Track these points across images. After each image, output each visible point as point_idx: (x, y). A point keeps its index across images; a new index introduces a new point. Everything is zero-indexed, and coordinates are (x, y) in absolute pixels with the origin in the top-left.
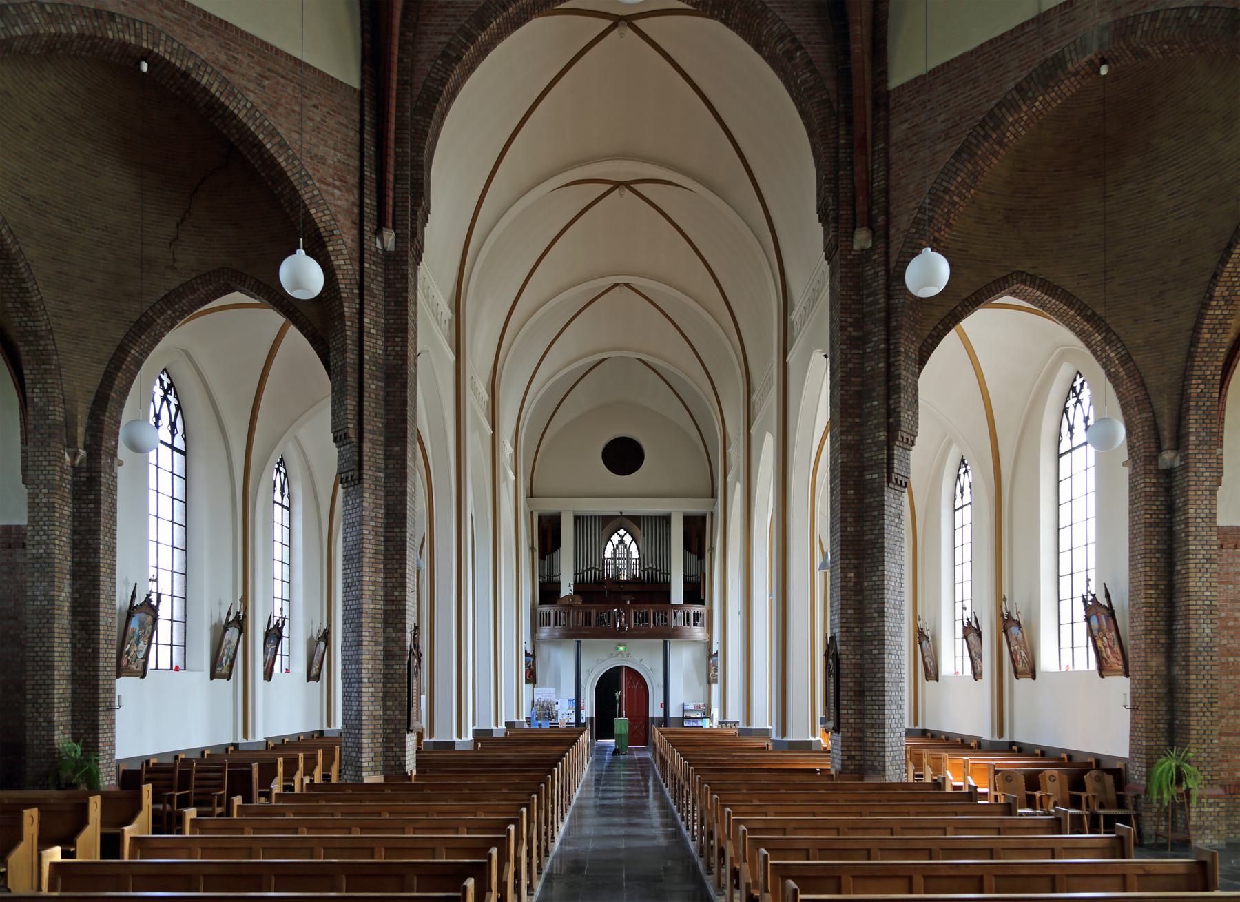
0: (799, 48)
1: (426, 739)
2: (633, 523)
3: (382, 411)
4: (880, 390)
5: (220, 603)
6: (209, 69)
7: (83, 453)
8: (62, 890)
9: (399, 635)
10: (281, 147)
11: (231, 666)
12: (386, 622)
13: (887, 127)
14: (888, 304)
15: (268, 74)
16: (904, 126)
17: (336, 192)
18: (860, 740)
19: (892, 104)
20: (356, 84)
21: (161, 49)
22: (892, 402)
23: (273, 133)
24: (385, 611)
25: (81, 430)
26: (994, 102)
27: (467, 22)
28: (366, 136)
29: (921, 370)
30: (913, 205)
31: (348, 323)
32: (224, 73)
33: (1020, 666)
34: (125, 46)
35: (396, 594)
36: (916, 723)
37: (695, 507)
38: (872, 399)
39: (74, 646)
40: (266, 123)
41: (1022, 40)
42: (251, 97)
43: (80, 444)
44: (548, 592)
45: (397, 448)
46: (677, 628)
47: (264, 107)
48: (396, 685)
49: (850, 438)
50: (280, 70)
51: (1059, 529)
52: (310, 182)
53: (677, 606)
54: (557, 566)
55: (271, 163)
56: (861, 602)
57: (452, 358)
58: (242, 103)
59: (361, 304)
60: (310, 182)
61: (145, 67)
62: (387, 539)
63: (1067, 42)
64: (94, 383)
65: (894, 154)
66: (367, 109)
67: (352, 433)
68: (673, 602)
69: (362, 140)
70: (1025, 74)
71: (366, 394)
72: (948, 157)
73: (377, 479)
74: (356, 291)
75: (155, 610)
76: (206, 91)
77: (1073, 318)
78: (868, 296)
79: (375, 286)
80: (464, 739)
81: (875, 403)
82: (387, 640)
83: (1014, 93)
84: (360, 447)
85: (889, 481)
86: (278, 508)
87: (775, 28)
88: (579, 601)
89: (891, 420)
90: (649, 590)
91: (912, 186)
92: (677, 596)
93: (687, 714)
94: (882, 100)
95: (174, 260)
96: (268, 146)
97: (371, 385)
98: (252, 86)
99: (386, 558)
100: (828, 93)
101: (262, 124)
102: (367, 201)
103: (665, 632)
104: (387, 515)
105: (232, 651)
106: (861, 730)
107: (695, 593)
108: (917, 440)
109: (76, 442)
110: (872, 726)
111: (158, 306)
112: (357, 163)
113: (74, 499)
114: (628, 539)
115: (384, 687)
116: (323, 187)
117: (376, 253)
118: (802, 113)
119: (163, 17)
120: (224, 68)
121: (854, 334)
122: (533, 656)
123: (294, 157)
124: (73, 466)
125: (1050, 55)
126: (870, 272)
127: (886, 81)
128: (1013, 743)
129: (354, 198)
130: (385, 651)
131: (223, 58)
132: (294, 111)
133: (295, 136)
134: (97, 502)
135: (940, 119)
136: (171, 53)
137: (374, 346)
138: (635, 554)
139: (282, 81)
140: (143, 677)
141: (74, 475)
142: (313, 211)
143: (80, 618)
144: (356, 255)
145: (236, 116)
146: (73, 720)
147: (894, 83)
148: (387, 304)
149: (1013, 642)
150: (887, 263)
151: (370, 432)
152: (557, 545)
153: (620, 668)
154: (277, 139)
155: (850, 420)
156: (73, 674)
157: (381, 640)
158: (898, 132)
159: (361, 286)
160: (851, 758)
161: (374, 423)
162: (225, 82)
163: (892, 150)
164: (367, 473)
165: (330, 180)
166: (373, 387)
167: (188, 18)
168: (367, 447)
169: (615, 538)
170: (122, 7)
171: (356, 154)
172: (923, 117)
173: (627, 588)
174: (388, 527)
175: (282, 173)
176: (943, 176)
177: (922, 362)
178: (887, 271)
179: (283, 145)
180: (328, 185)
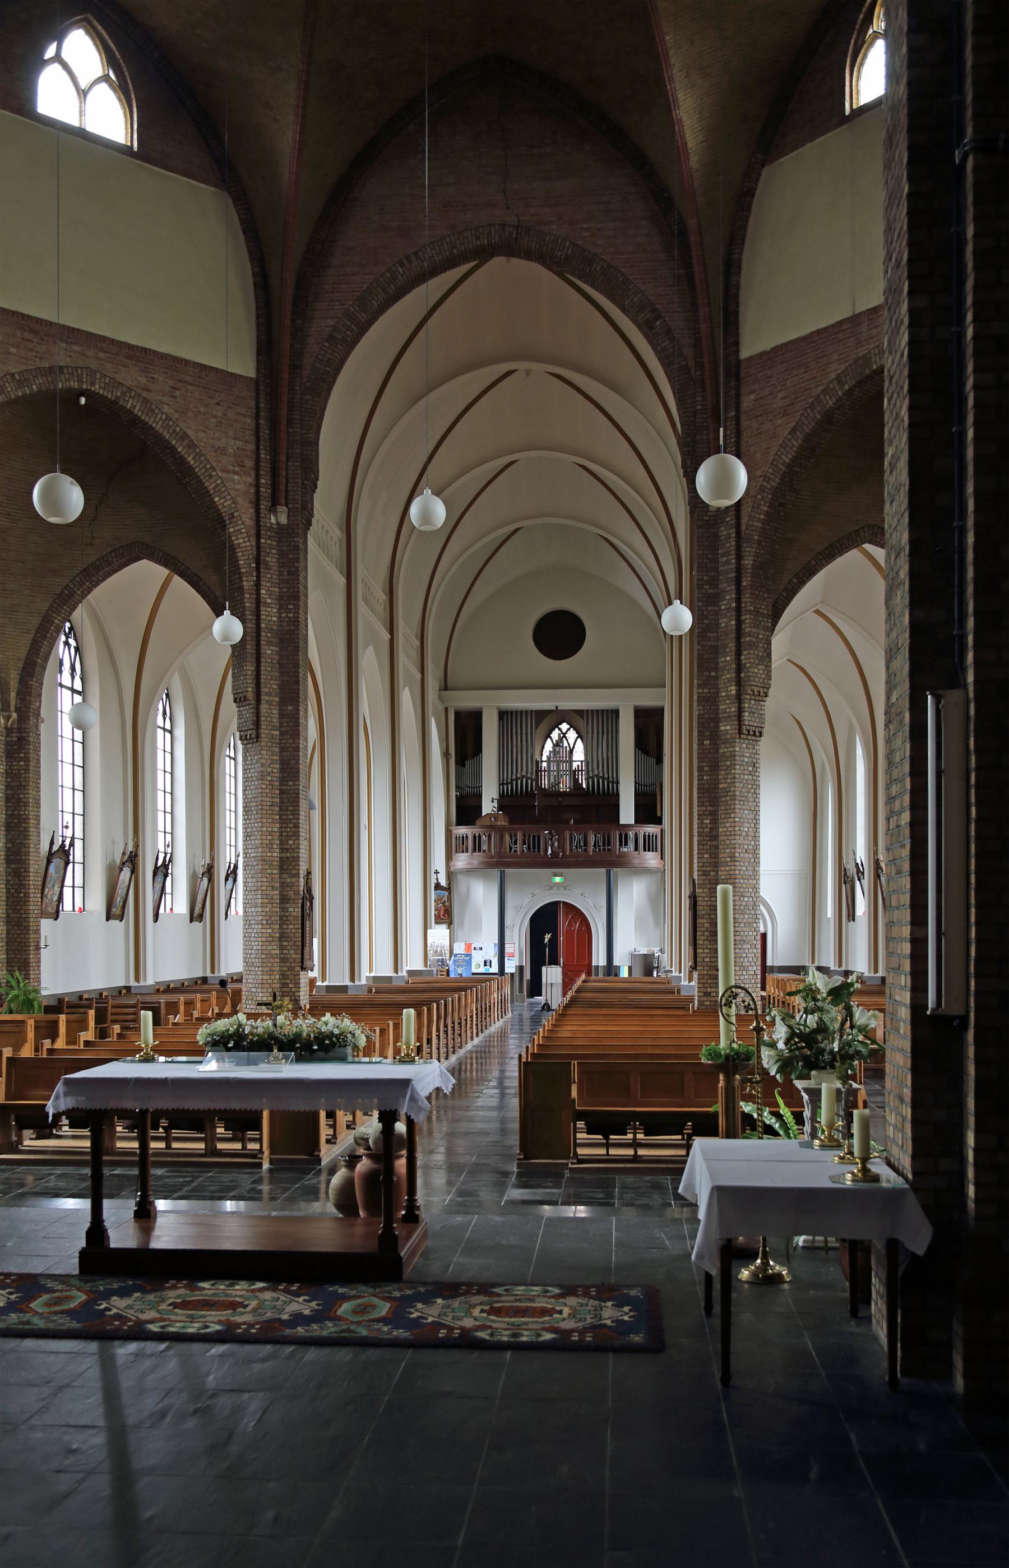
1: (319, 983)
2: (576, 718)
3: (277, 674)
4: (732, 645)
5: (113, 843)
6: (133, 394)
7: (15, 715)
9: (294, 880)
10: (190, 448)
11: (124, 907)
12: (282, 869)
13: (738, 396)
15: (179, 385)
16: (752, 397)
17: (236, 477)
19: (743, 374)
20: (252, 373)
21: (97, 386)
23: (184, 436)
24: (281, 858)
25: (13, 695)
26: (820, 388)
27: (351, 305)
28: (261, 422)
29: (775, 624)
31: (247, 596)
32: (145, 394)
34: (70, 390)
35: (290, 842)
36: (840, 965)
37: (648, 699)
38: (726, 654)
39: (8, 891)
40: (178, 429)
41: (840, 336)
42: (166, 409)
43: (12, 708)
44: (466, 810)
45: (290, 708)
47: (176, 416)
48: (291, 927)
49: (706, 690)
50: (189, 379)
52: (214, 474)
54: (478, 775)
55: (182, 461)
56: (717, 847)
57: (342, 580)
58: (159, 417)
59: (258, 576)
60: (214, 474)
61: (83, 401)
62: (282, 792)
63: (872, 346)
64: (23, 652)
65: (744, 423)
66: (262, 396)
67: (251, 695)
68: (623, 821)
69: (258, 425)
70: (843, 367)
71: (263, 660)
72: (786, 432)
73: (273, 737)
74: (254, 565)
75: (67, 854)
76: (130, 412)
77: (272, 956)
79: (271, 559)
80: (357, 983)
81: (728, 658)
82: (283, 885)
83: (835, 383)
84: (257, 708)
85: (740, 733)
86: (160, 732)
87: (636, 299)
88: (502, 822)
90: (594, 804)
91: (758, 455)
92: (627, 814)
94: (735, 369)
95: (93, 538)
96: (179, 450)
98: (165, 400)
99: (281, 810)
101: (174, 431)
102: (263, 481)
103: (608, 861)
104: (282, 770)
105: (125, 891)
107: (648, 810)
108: (771, 692)
109: (9, 707)
111: (78, 579)
112: (253, 447)
113: (7, 757)
114: (572, 735)
115: (280, 928)
116: (225, 475)
119: (98, 359)
120: (144, 389)
121: (710, 591)
122: (449, 889)
123: (201, 454)
124: (6, 728)
125: (861, 354)
127: (737, 351)
129: (250, 480)
131: (143, 380)
132: (200, 412)
133: (202, 435)
134: (27, 760)
135: (780, 395)
136: (104, 388)
138: (579, 754)
139: (190, 388)
140: (56, 919)
141: (7, 736)
142: (217, 499)
143: (13, 866)
144: (253, 532)
145: (153, 429)
146: (7, 958)
147: (745, 354)
148: (281, 574)
150: (738, 526)
151: (267, 694)
152: (478, 750)
153: (558, 902)
154: (186, 442)
156: (8, 916)
157: (277, 885)
158: (747, 402)
159: (258, 562)
160: (707, 994)
161: (270, 685)
162: (146, 400)
163: (743, 417)
164: (264, 731)
165: (231, 468)
166: (269, 652)
167: (117, 354)
168: (264, 708)
169: (555, 735)
170: (68, 359)
171: (252, 439)
172: (767, 391)
173: (568, 801)
174: (283, 781)
175: (191, 469)
176: (782, 450)
177: (776, 615)
178: (738, 533)
179: (192, 446)
180: (229, 472)
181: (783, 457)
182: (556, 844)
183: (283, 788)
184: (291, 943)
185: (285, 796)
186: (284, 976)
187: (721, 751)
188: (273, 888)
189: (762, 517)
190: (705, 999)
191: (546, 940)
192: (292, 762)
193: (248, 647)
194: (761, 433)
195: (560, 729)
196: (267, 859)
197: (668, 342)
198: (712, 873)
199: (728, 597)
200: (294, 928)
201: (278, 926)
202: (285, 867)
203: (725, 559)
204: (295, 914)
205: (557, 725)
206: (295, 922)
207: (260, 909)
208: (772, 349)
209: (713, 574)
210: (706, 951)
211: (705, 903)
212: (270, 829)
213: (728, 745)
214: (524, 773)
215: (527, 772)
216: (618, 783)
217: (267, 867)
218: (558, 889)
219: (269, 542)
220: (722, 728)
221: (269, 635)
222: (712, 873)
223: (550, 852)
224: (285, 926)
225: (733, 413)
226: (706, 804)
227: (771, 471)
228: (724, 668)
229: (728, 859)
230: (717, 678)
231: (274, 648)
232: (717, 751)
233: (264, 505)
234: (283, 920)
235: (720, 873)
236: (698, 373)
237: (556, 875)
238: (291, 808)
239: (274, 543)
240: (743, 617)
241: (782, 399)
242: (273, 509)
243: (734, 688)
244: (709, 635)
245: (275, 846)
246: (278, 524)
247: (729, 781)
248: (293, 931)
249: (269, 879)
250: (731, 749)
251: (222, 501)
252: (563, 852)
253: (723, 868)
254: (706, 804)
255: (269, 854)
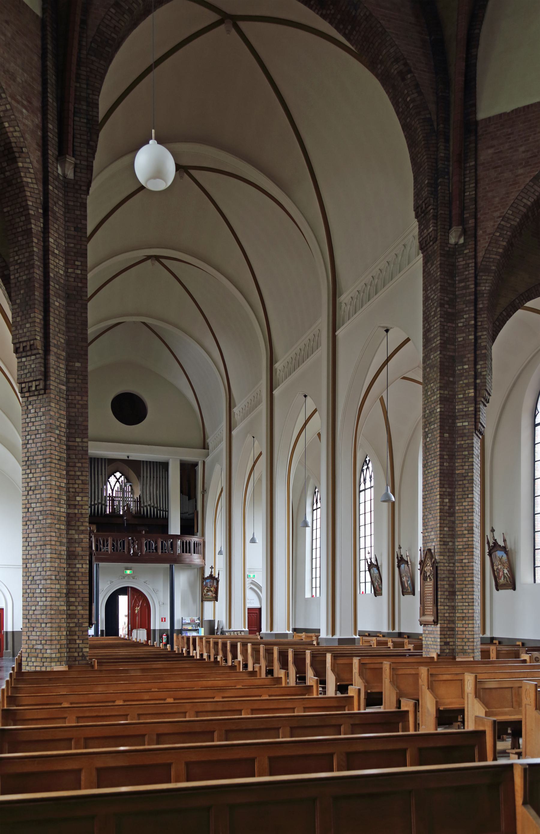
0: (410, 71)
3: (64, 328)
4: (471, 356)
8: (403, 731)
14: (476, 290)
16: (490, 151)
17: (24, 111)
18: (453, 629)
22: (479, 367)
24: (68, 514)
30: (497, 214)
31: (35, 240)
33: (502, 581)
35: (78, 498)
37: (190, 456)
45: (78, 364)
46: (179, 556)
48: (79, 583)
49: (446, 392)
51: (534, 480)
53: (175, 537)
56: (454, 522)
62: (69, 448)
72: (528, 180)
78: (461, 281)
79: (57, 209)
81: (466, 367)
87: (392, 50)
89: (478, 381)
91: (497, 199)
92: (175, 528)
93: (185, 627)
94: (470, 126)
97: (56, 303)
99: (68, 465)
100: (430, 114)
104: (69, 425)
106: (453, 622)
110: (463, 618)
115: (68, 584)
117: (57, 178)
118: (406, 127)
121: (449, 310)
126: (461, 262)
127: (475, 113)
128: (492, 639)
129: (38, 120)
130: (68, 551)
137: (57, 265)
144: (40, 176)
147: (481, 115)
149: (496, 563)
151: (55, 346)
153: (128, 587)
155: (446, 378)
157: (65, 540)
158: (485, 155)
160: (447, 644)
164: (53, 383)
165: (19, 98)
168: (52, 359)
174: (70, 437)
180: (18, 102)
181: (525, 201)
182: (136, 546)
183: (70, 443)
184: (78, 599)
185: (71, 452)
186: (70, 632)
187: (458, 443)
188: (61, 544)
189: (501, 250)
190: (445, 647)
191: (136, 611)
192: (80, 419)
193: (36, 293)
194: (500, 181)
195: (115, 476)
196: (56, 513)
197: (416, 95)
198: (450, 544)
199: (465, 316)
200: (81, 584)
201: (65, 582)
202: (73, 523)
203: (463, 284)
204: (83, 570)
205: (113, 474)
206: (83, 578)
207: (48, 564)
208: (512, 111)
209: (451, 296)
210: (446, 608)
211: (445, 568)
212: (58, 484)
213: (465, 438)
214: (100, 501)
215: (102, 500)
216: (168, 511)
217: (56, 522)
218: (129, 578)
219: (56, 192)
220: (459, 424)
221: (57, 286)
222: (450, 544)
223: (132, 552)
224: (72, 583)
225: (473, 163)
226: (446, 486)
227: (511, 212)
228: (462, 375)
229: (466, 532)
230: (454, 383)
231: (61, 301)
232: (454, 442)
233: (52, 152)
234: (70, 576)
235: (457, 544)
236: (442, 126)
237: (127, 569)
238: (79, 465)
239: (61, 195)
240: (479, 334)
241: (524, 152)
242: (61, 154)
243: (472, 391)
244: (448, 346)
245: (63, 502)
246: (65, 176)
247: (467, 467)
248: (81, 587)
249: (58, 534)
250: (468, 441)
251: (12, 129)
252: (141, 552)
253: (459, 540)
254: (446, 486)
255: (58, 509)
